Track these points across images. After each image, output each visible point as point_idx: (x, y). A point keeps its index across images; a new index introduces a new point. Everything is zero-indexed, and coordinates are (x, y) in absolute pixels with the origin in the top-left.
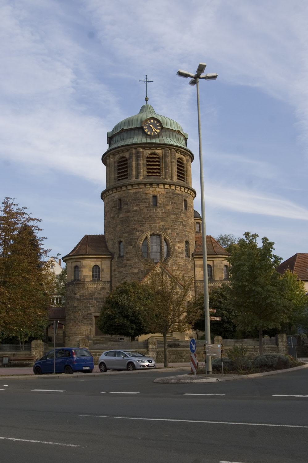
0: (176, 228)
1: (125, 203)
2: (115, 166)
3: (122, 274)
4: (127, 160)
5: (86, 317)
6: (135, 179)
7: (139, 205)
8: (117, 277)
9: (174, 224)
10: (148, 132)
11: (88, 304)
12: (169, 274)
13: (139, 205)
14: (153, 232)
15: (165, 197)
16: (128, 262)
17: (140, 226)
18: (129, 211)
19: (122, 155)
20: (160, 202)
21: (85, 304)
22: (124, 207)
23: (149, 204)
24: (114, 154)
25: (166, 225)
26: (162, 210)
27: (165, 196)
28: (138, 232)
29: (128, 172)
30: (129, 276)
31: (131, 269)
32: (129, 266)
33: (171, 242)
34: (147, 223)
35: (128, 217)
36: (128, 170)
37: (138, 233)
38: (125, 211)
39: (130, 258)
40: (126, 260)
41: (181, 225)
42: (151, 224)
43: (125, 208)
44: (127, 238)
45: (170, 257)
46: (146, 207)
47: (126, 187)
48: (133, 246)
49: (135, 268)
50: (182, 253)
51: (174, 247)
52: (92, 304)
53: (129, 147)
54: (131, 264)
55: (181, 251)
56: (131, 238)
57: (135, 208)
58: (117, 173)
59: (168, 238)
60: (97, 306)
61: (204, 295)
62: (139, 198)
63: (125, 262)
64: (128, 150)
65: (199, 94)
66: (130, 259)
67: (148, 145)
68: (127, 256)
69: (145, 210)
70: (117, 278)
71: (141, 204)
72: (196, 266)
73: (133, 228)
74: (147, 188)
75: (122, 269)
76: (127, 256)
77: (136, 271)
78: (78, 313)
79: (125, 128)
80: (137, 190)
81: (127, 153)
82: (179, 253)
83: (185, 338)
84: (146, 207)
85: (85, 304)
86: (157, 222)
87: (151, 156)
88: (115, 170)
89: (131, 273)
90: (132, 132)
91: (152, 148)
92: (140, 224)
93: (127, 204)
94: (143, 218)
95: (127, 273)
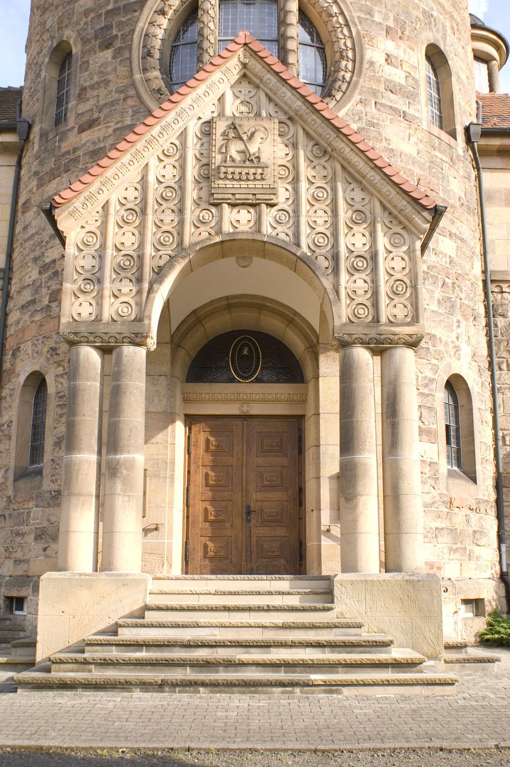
16: (86, 136)
32: (87, 159)
33: (341, 20)
39: (95, 116)
40: (76, 130)
44: (92, 15)
45: (338, 96)
48: (118, 44)
50: (411, 97)
55: (403, 82)
56: (110, 7)
61: (129, 452)
65: (489, 238)
66: (98, 118)
72: (490, 198)
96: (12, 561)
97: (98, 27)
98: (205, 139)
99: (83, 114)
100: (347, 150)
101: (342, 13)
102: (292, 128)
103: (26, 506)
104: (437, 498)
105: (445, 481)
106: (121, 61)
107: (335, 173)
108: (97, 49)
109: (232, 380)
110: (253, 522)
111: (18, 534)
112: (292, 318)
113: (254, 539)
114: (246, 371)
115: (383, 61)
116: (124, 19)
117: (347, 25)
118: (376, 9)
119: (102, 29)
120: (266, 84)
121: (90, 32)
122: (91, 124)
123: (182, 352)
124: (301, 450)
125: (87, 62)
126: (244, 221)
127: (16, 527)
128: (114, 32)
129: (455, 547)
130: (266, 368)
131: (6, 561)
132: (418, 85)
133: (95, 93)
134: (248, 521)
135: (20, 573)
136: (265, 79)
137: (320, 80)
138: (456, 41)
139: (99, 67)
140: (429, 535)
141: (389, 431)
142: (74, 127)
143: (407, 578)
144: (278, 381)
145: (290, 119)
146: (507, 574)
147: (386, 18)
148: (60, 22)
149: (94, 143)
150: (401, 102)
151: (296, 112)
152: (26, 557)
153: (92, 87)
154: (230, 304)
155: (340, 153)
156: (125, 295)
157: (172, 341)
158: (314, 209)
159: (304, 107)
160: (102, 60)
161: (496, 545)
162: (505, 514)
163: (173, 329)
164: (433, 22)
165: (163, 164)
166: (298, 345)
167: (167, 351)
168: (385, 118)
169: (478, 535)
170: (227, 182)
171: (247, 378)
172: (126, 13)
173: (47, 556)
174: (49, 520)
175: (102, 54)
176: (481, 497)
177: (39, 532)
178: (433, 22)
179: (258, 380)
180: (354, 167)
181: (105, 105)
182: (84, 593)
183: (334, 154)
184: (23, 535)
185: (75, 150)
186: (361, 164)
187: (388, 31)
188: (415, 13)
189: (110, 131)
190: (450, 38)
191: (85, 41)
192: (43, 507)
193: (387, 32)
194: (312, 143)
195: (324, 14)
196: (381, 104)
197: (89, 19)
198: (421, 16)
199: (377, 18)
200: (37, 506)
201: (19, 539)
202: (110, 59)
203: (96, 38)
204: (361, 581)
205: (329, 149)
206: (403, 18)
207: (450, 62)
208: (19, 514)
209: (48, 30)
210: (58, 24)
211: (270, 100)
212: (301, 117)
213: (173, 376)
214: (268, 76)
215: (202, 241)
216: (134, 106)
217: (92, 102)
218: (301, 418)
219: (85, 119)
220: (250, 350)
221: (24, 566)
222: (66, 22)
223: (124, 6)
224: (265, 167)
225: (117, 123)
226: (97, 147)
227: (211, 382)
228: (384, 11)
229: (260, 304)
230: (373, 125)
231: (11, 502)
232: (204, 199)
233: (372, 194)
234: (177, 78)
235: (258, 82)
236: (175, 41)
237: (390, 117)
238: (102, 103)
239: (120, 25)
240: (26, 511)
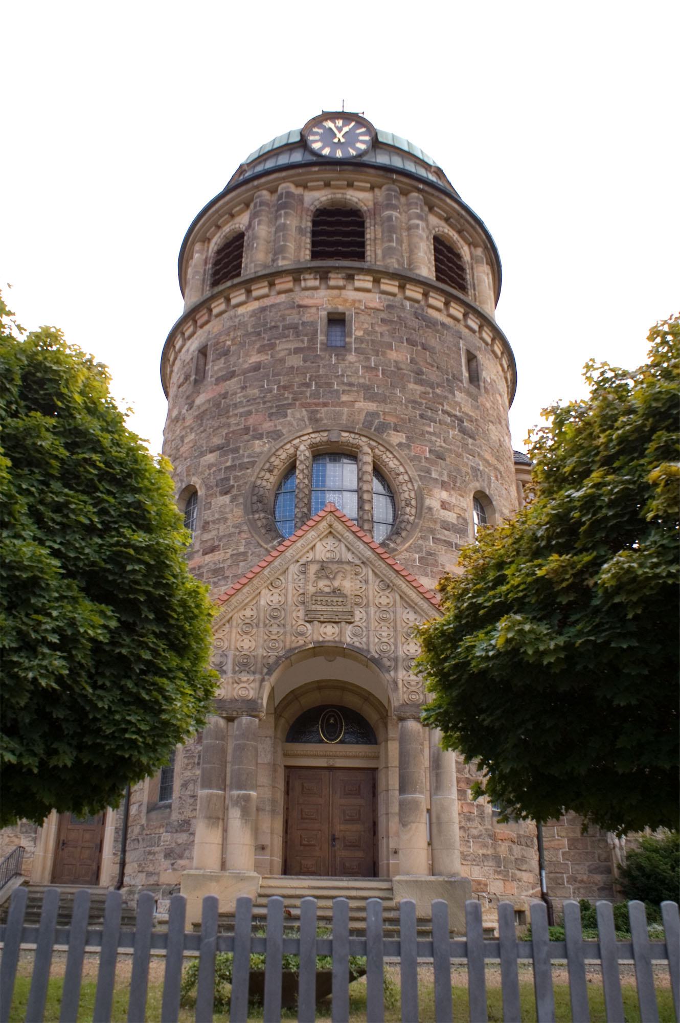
0: (431, 430)
1: (219, 354)
9: (422, 416)
13: (272, 346)
15: (383, 320)
16: (208, 558)
17: (271, 415)
20: (360, 333)
22: (213, 366)
25: (384, 413)
26: (368, 359)
27: (383, 315)
33: (406, 477)
34: (297, 403)
35: (225, 396)
39: (216, 543)
40: (201, 553)
41: (453, 428)
42: (317, 405)
44: (214, 469)
46: (297, 351)
48: (234, 492)
51: (420, 498)
55: (455, 521)
56: (229, 464)
59: (393, 463)
62: (273, 324)
66: (219, 546)
69: (296, 361)
71: (277, 342)
73: (242, 426)
80: (266, 302)
82: (446, 526)
83: (484, 917)
92: (271, 407)
93: (226, 353)
94: (285, 388)
96: (145, 874)
97: (218, 478)
98: (302, 576)
99: (206, 541)
100: (404, 586)
101: (407, 472)
102: (364, 569)
103: (157, 832)
104: (484, 832)
105: (490, 819)
106: (236, 504)
107: (395, 601)
108: (218, 494)
109: (322, 741)
110: (338, 846)
111: (150, 853)
112: (367, 697)
113: (338, 860)
114: (332, 734)
115: (439, 507)
116: (239, 474)
117: (411, 481)
118: (433, 468)
119: (222, 480)
120: (346, 539)
121: (212, 481)
122: (213, 549)
123: (282, 721)
124: (374, 794)
125: (210, 503)
126: (329, 633)
127: (148, 848)
128: (232, 482)
129: (499, 869)
130: (348, 733)
131: (140, 874)
132: (467, 523)
133: (217, 526)
134: (334, 846)
135: (152, 882)
136: (345, 535)
137: (390, 520)
138: (499, 485)
139: (220, 508)
140: (477, 859)
141: (434, 779)
142: (199, 551)
143: (446, 879)
144: (357, 743)
145: (363, 563)
146: (547, 894)
147: (441, 474)
148: (188, 470)
149: (215, 563)
150: (453, 536)
151: (368, 559)
152: (157, 871)
153: (214, 522)
154: (320, 686)
155: (399, 587)
156: (244, 682)
157: (275, 712)
158: (380, 626)
159: (373, 556)
160: (221, 503)
161: (537, 871)
162: (545, 847)
163: (276, 704)
164: (479, 474)
165: (271, 592)
166: (372, 716)
167: (272, 719)
168: (441, 550)
169: (519, 862)
170: (318, 607)
171: (333, 740)
172: (241, 470)
173: (174, 870)
174: (176, 843)
175: (221, 498)
176: (522, 832)
177: (168, 851)
178: (479, 474)
179: (342, 742)
180: (409, 597)
181: (224, 536)
182: (214, 884)
183: (395, 588)
184: (154, 854)
185: (200, 567)
186: (413, 595)
187: (443, 483)
188: (464, 469)
189: (228, 555)
190: (494, 483)
191: (208, 487)
192: (172, 832)
193: (442, 485)
194: (379, 580)
195: (393, 473)
196: (437, 539)
197: (212, 471)
198: (470, 471)
199: (434, 475)
200: (167, 832)
201: (151, 857)
202: (228, 502)
203: (217, 486)
204: (413, 881)
205: (391, 584)
206: (455, 474)
207: (494, 503)
208: (151, 839)
209: (178, 474)
210: (187, 472)
211: (349, 549)
212: (371, 562)
213: (275, 738)
214: (348, 534)
215: (300, 647)
216: (247, 538)
217: (214, 533)
218: (375, 770)
219: (209, 544)
220: (335, 720)
221: (156, 878)
222: (193, 471)
223: (239, 464)
224: (345, 596)
225: (233, 550)
226: (217, 566)
227: (305, 742)
228: (439, 469)
229: (343, 687)
230: (431, 554)
231: (144, 829)
232: (301, 618)
233: (422, 616)
234: (280, 517)
235: (340, 537)
236: (278, 490)
237: (444, 548)
238: (221, 534)
239: (236, 478)
240: (157, 836)
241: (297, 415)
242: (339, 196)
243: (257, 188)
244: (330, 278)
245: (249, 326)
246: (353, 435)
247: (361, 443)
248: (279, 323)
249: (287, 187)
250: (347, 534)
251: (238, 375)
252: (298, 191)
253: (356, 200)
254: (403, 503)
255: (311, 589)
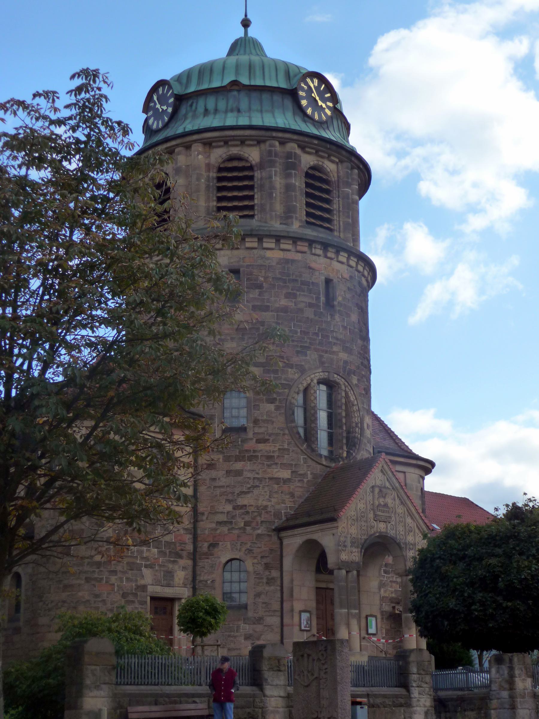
2: (208, 176)
3: (240, 479)
4: (251, 168)
5: (131, 598)
6: (281, 224)
7: (295, 296)
8: (222, 487)
10: (307, 107)
11: (137, 557)
12: (401, 491)
13: (295, 296)
14: (327, 374)
16: (261, 446)
18: (268, 306)
19: (235, 151)
21: (131, 557)
23: (318, 298)
24: (209, 144)
28: (292, 368)
29: (256, 201)
30: (263, 488)
31: (269, 466)
36: (256, 196)
37: (290, 370)
38: (253, 306)
39: (267, 437)
40: (254, 440)
42: (323, 351)
43: (251, 296)
46: (310, 305)
47: (260, 240)
48: (277, 403)
49: (284, 466)
52: (147, 559)
53: (268, 134)
54: (272, 454)
57: (284, 302)
58: (215, 198)
59: (352, 398)
60: (160, 566)
62: (294, 277)
63: (251, 445)
64: (259, 142)
66: (268, 440)
67: (316, 142)
68: (257, 430)
69: (309, 313)
70: (222, 490)
71: (298, 293)
74: (315, 255)
75: (238, 466)
76: (257, 430)
77: (286, 474)
78: (107, 582)
79: (245, 80)
81: (254, 148)
84: (310, 305)
85: (131, 557)
86: (335, 349)
87: (230, 165)
88: (208, 187)
89: (271, 479)
90: (266, 96)
91: (320, 153)
92: (297, 346)
93: (260, 287)
95: (258, 479)
120: (388, 475)
122: (265, 441)
151: (396, 487)
180: (411, 511)
241: (312, 356)
242: (320, 163)
243: (274, 138)
244: (329, 251)
245: (277, 271)
246: (338, 377)
247: (341, 383)
248: (298, 278)
249: (292, 147)
250: (389, 472)
251: (272, 311)
252: (298, 151)
253: (329, 170)
254: (354, 425)
255: (377, 503)
